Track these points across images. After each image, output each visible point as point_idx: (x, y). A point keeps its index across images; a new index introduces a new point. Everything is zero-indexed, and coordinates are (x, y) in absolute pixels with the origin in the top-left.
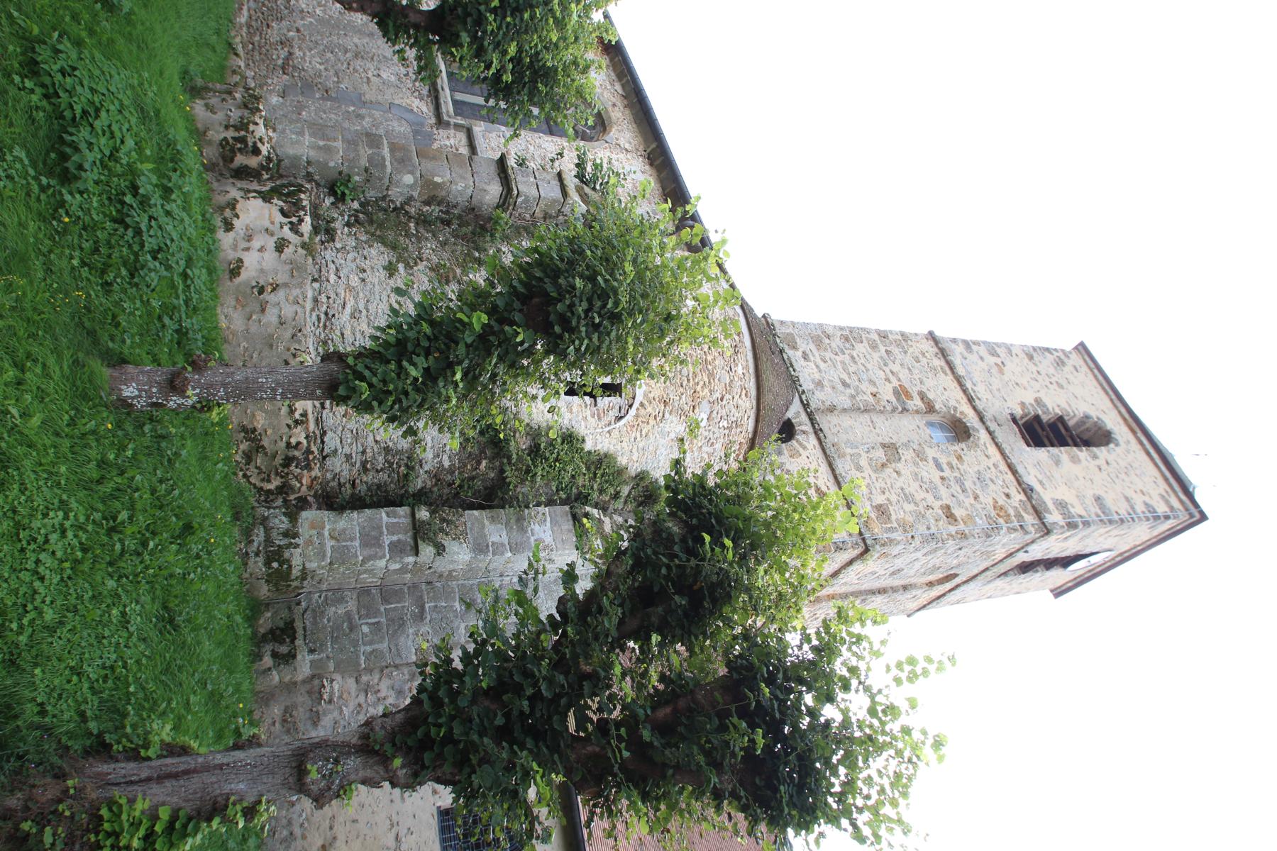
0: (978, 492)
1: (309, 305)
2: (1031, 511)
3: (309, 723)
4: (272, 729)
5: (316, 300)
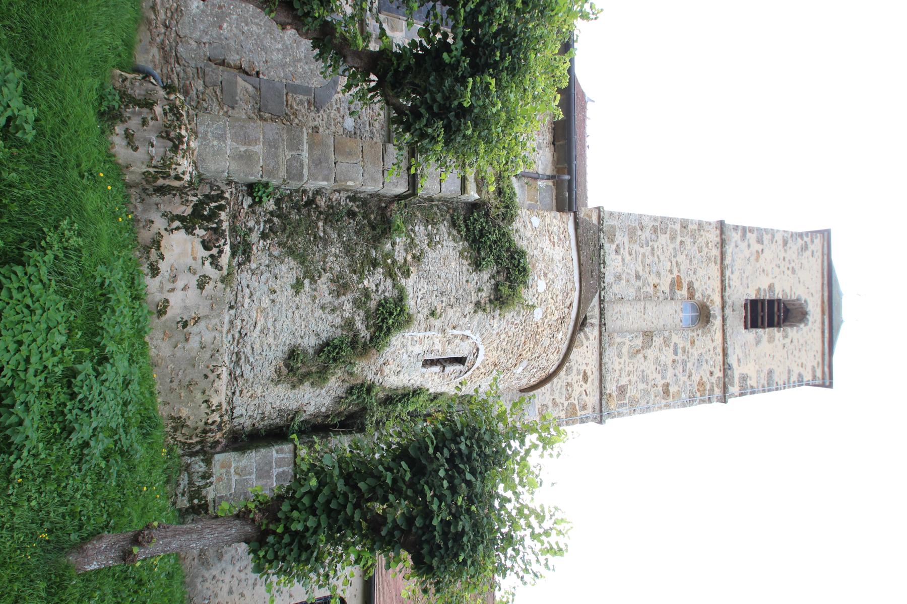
0: (693, 371)
1: (226, 327)
2: (721, 385)
3: (216, 558)
4: (193, 563)
5: (231, 322)
